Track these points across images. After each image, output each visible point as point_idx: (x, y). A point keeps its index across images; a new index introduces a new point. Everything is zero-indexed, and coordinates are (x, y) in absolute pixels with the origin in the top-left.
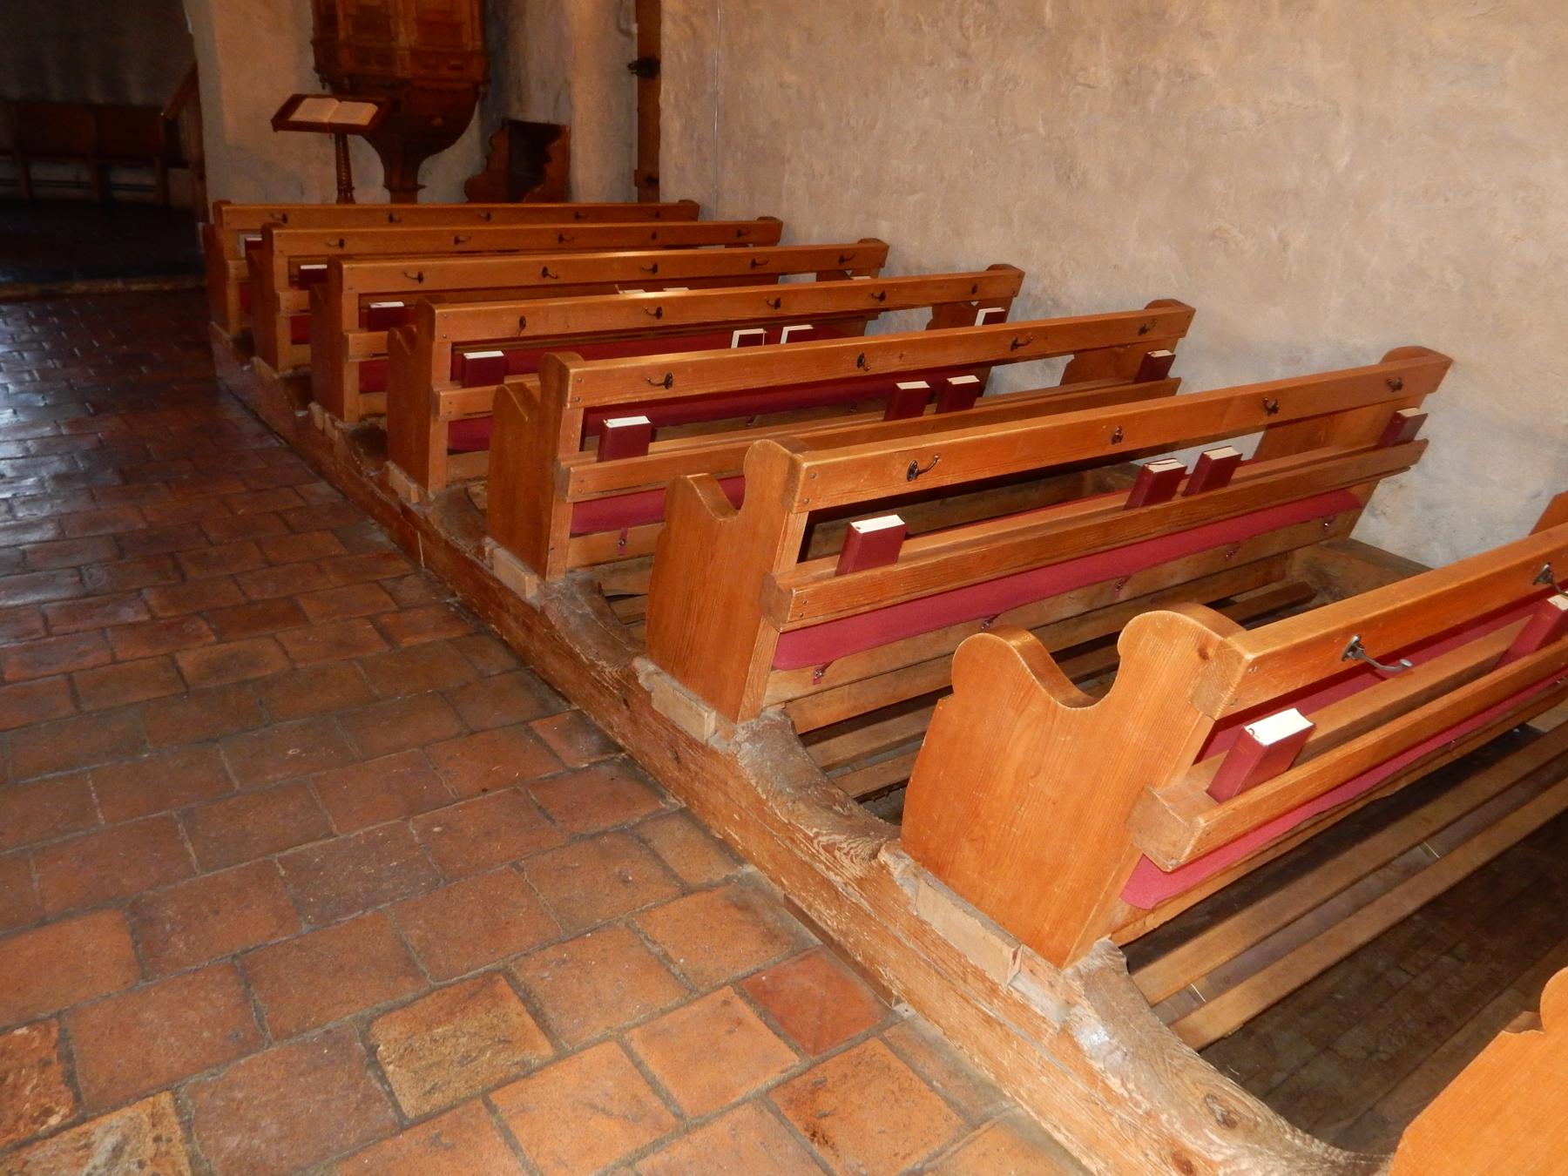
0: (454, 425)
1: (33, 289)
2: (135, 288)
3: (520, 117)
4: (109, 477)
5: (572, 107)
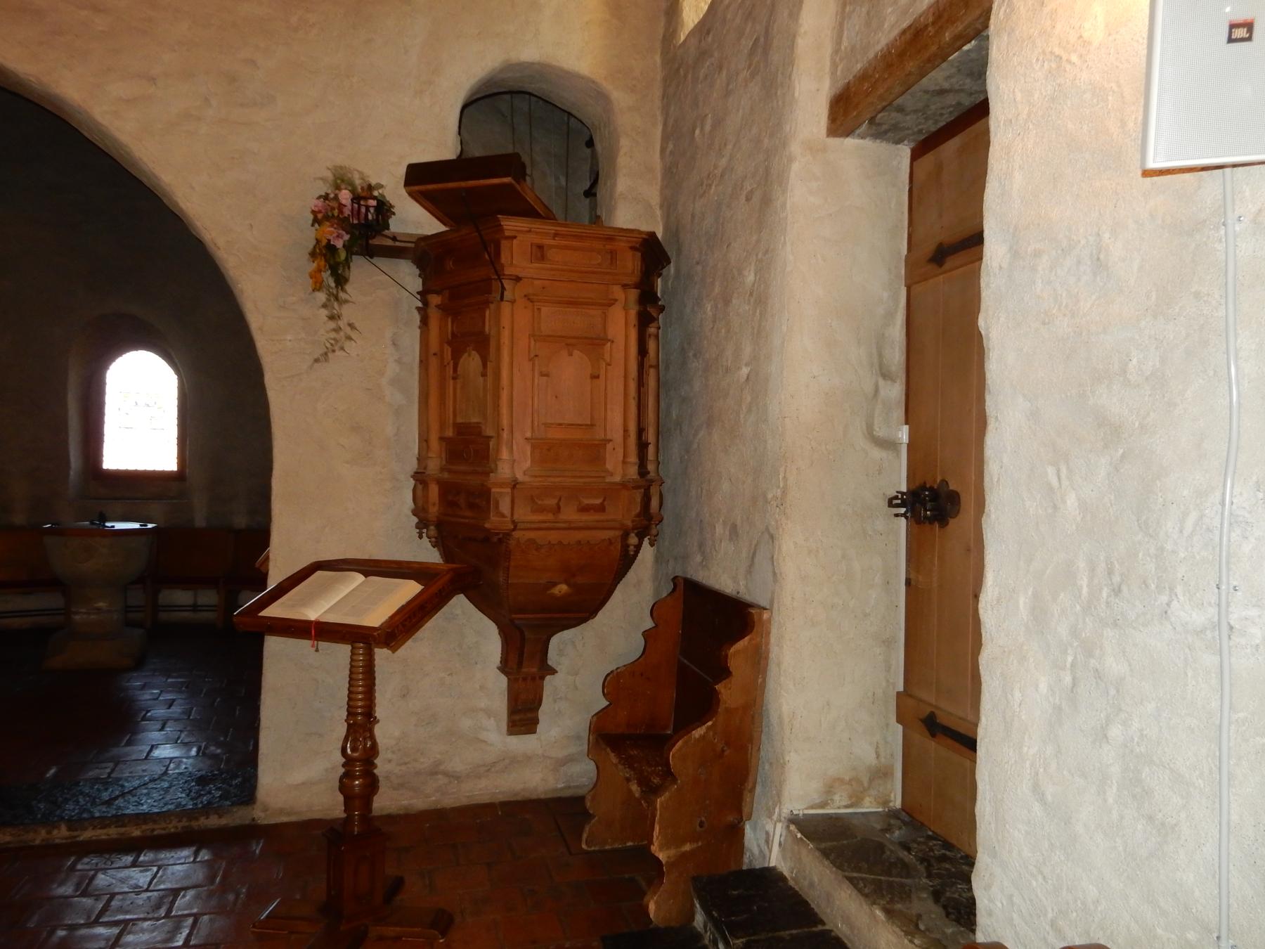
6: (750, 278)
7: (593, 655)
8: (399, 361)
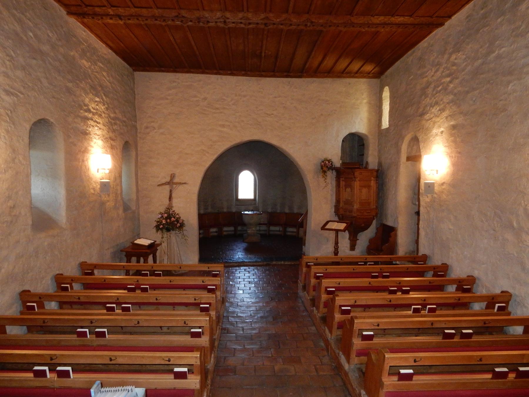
0: (339, 323)
1: (265, 263)
2: (286, 263)
4: (270, 319)
5: (398, 223)
6: (394, 178)
7: (365, 238)
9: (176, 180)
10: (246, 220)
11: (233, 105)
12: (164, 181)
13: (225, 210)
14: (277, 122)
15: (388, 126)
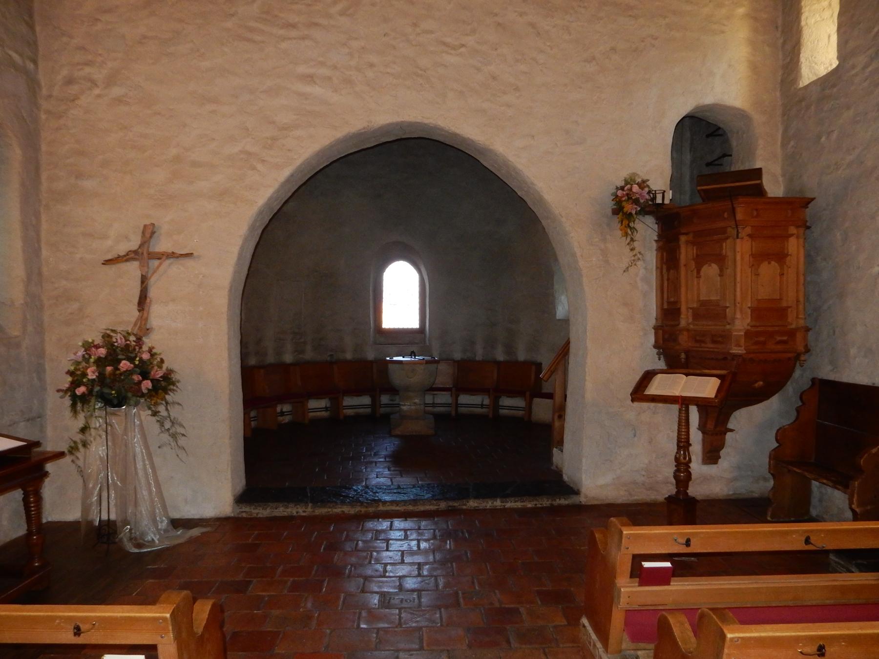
1: (443, 505)
2: (508, 505)
3: (832, 377)
8: (646, 268)
9: (162, 245)
10: (397, 378)
11: (341, 15)
12: (123, 248)
13: (349, 356)
14: (478, 70)
15: (835, 63)
